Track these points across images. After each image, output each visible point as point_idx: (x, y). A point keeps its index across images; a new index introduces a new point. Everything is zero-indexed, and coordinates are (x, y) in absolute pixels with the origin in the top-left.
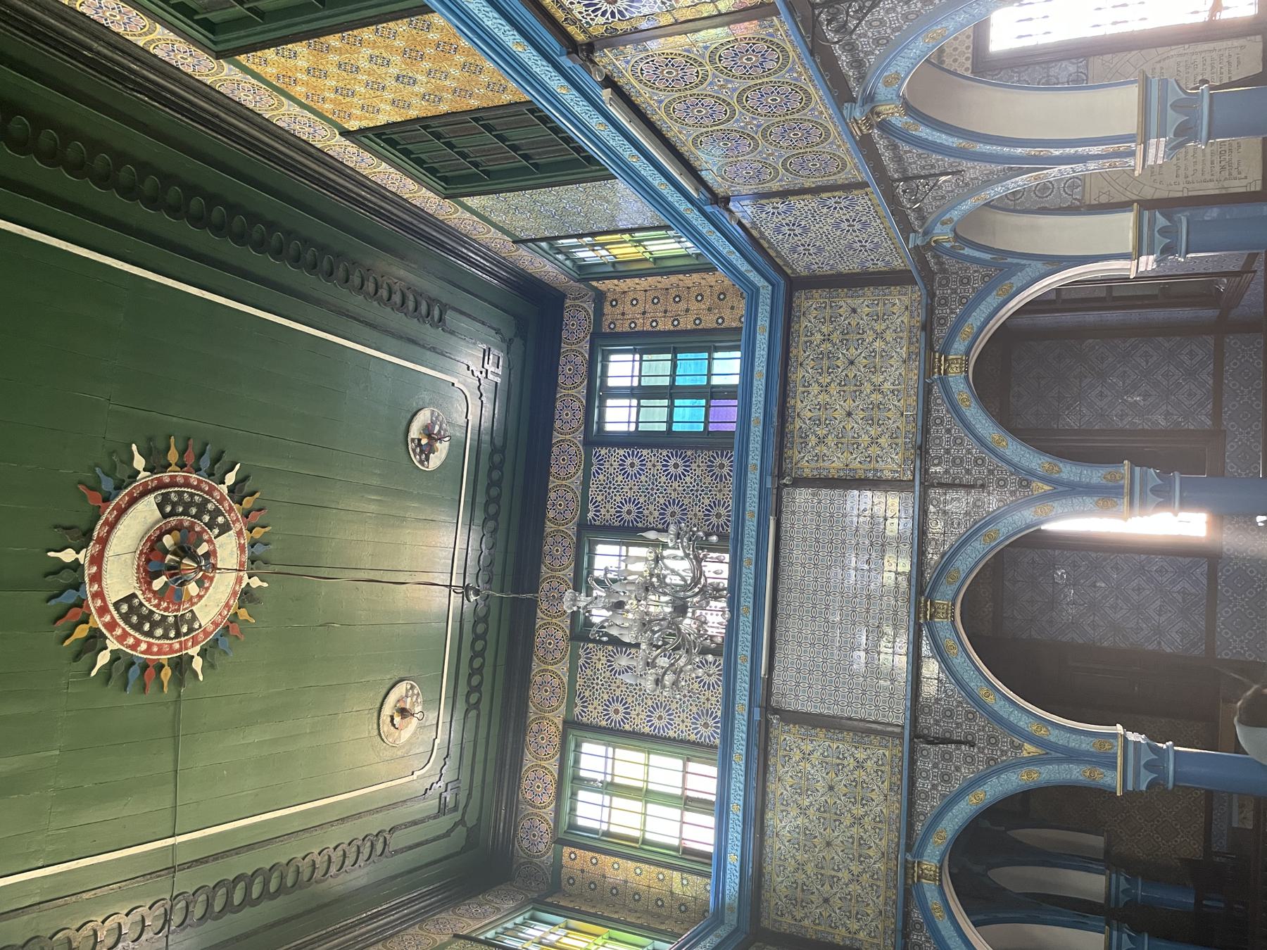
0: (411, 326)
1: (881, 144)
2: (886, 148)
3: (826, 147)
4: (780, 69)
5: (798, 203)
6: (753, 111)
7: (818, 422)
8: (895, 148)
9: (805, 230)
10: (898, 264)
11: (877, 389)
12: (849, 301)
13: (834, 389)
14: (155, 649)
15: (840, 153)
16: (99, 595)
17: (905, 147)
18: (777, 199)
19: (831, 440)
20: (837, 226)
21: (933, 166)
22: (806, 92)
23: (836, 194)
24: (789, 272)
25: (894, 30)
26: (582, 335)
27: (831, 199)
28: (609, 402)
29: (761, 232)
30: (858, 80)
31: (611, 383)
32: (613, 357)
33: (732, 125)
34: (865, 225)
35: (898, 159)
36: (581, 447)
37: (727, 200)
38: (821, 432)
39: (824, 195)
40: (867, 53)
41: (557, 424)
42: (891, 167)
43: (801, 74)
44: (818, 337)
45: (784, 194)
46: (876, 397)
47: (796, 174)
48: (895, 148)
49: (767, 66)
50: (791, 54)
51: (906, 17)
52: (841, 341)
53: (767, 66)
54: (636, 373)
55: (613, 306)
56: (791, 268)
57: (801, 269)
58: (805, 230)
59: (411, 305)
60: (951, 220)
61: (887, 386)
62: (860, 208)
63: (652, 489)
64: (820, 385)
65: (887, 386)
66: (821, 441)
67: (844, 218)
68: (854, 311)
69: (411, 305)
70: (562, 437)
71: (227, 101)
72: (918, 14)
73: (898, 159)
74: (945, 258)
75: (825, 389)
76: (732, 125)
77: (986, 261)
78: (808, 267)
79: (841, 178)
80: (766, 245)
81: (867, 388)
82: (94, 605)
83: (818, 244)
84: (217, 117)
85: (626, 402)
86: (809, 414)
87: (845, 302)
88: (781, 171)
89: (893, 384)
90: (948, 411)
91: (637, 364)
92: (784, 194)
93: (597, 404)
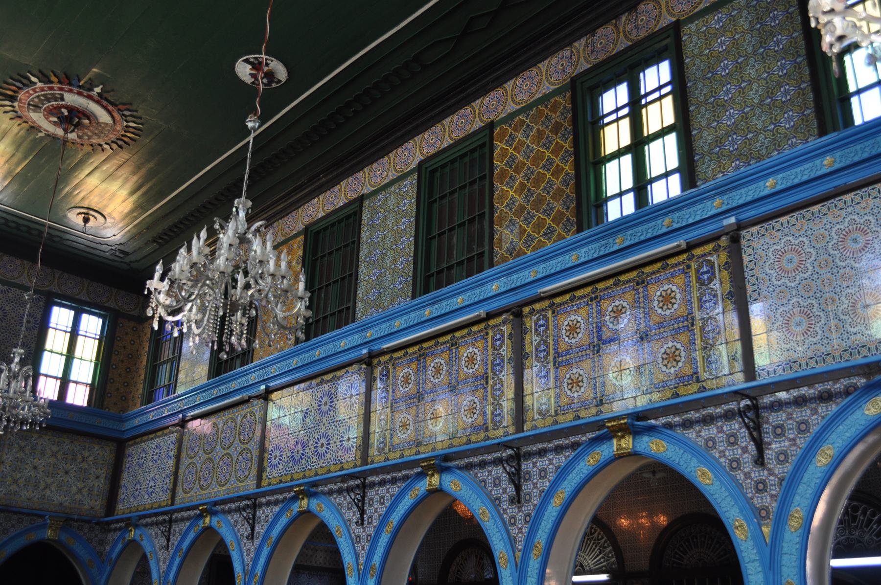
0: (160, 229)
1: (191, 513)
2: (189, 515)
3: (197, 487)
4: (236, 477)
5: (171, 463)
6: (222, 458)
7: (34, 448)
8: (188, 519)
9: (155, 462)
10: (120, 507)
11: (47, 486)
12: (104, 475)
13: (52, 460)
14: (31, 92)
15: (192, 493)
16: (70, 91)
17: (187, 524)
18: (176, 453)
19: (20, 455)
20: (153, 479)
21: (174, 535)
22: (224, 485)
23: (172, 484)
24: (130, 443)
25: (239, 529)
26: (120, 304)
27: (169, 481)
28: (72, 312)
29: (159, 437)
30: (223, 509)
31: (85, 317)
32: (101, 320)
33: (218, 446)
34: (150, 494)
35: (182, 520)
36: (47, 289)
37: (369, 364)
38: (27, 450)
39: (172, 478)
40: (232, 516)
41: (66, 275)
42: (179, 515)
43: (232, 485)
44: (86, 454)
45: (178, 458)
46: (42, 485)
47: (187, 467)
48: (188, 519)
49: (239, 472)
50: (241, 484)
51: (242, 535)
52: (81, 468)
53: (239, 472)
54: (88, 334)
55: (133, 327)
56: (132, 445)
57: (130, 450)
58: (155, 462)
59: (169, 233)
60: (142, 540)
61: (48, 492)
62: (160, 494)
63: (10, 333)
64: (57, 452)
65: (48, 492)
66: (21, 449)
67: (157, 484)
68: (97, 477)
69: (169, 233)
70: (57, 276)
71: (289, 211)
72: (242, 540)
73: (182, 520)
74: (118, 534)
75: (54, 455)
76: (218, 446)
77: (169, 576)
78: (131, 455)
79: (179, 489)
80: (151, 436)
81: (49, 480)
82: (66, 87)
83: (144, 465)
84: (285, 201)
85: (70, 325)
86: (40, 443)
87: (104, 473)
88: (191, 461)
89: (49, 496)
90: (25, 526)
91: (94, 336)
92: (178, 458)
93: (73, 305)
